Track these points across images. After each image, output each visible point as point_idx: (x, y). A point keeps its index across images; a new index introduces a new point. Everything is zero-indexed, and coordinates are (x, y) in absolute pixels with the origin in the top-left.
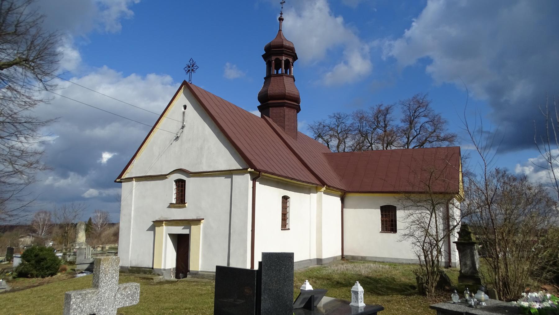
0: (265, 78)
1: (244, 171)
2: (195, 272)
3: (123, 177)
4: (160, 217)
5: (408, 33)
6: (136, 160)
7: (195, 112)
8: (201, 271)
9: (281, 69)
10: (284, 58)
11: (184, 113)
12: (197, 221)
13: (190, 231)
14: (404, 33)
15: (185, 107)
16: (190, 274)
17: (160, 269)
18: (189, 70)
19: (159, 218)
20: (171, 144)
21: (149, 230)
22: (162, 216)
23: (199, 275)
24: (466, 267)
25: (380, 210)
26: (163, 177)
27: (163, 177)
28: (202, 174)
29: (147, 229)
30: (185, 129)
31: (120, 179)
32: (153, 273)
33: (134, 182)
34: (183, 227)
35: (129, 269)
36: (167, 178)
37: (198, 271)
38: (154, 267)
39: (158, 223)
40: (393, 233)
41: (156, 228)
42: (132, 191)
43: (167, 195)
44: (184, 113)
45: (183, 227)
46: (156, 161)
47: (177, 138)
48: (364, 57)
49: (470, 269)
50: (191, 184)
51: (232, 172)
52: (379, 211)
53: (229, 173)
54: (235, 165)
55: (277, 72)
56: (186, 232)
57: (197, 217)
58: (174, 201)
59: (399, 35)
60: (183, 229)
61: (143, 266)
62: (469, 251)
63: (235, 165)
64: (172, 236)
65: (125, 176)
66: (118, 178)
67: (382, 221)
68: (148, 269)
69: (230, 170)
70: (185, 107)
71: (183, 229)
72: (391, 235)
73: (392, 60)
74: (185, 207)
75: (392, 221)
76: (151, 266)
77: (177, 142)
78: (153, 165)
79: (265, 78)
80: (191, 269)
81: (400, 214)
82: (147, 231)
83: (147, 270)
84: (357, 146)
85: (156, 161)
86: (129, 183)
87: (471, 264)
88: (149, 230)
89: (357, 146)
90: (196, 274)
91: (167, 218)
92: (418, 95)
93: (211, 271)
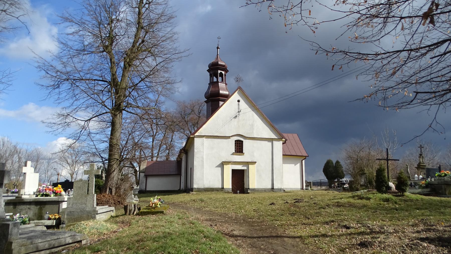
0: (209, 84)
3: (195, 135)
7: (246, 105)
10: (219, 71)
11: (239, 104)
13: (248, 168)
15: (239, 101)
16: (250, 190)
17: (229, 188)
18: (237, 81)
22: (227, 159)
26: (229, 137)
27: (229, 137)
29: (216, 166)
30: (240, 113)
33: (204, 139)
35: (204, 189)
36: (230, 138)
39: (228, 163)
44: (239, 104)
46: (221, 128)
47: (236, 116)
50: (247, 144)
53: (271, 140)
54: (274, 136)
56: (245, 168)
58: (234, 152)
62: (363, 176)
63: (274, 136)
64: (234, 171)
69: (272, 139)
70: (239, 101)
74: (244, 155)
79: (209, 84)
84: (102, 160)
85: (221, 128)
89: (102, 160)
90: (254, 190)
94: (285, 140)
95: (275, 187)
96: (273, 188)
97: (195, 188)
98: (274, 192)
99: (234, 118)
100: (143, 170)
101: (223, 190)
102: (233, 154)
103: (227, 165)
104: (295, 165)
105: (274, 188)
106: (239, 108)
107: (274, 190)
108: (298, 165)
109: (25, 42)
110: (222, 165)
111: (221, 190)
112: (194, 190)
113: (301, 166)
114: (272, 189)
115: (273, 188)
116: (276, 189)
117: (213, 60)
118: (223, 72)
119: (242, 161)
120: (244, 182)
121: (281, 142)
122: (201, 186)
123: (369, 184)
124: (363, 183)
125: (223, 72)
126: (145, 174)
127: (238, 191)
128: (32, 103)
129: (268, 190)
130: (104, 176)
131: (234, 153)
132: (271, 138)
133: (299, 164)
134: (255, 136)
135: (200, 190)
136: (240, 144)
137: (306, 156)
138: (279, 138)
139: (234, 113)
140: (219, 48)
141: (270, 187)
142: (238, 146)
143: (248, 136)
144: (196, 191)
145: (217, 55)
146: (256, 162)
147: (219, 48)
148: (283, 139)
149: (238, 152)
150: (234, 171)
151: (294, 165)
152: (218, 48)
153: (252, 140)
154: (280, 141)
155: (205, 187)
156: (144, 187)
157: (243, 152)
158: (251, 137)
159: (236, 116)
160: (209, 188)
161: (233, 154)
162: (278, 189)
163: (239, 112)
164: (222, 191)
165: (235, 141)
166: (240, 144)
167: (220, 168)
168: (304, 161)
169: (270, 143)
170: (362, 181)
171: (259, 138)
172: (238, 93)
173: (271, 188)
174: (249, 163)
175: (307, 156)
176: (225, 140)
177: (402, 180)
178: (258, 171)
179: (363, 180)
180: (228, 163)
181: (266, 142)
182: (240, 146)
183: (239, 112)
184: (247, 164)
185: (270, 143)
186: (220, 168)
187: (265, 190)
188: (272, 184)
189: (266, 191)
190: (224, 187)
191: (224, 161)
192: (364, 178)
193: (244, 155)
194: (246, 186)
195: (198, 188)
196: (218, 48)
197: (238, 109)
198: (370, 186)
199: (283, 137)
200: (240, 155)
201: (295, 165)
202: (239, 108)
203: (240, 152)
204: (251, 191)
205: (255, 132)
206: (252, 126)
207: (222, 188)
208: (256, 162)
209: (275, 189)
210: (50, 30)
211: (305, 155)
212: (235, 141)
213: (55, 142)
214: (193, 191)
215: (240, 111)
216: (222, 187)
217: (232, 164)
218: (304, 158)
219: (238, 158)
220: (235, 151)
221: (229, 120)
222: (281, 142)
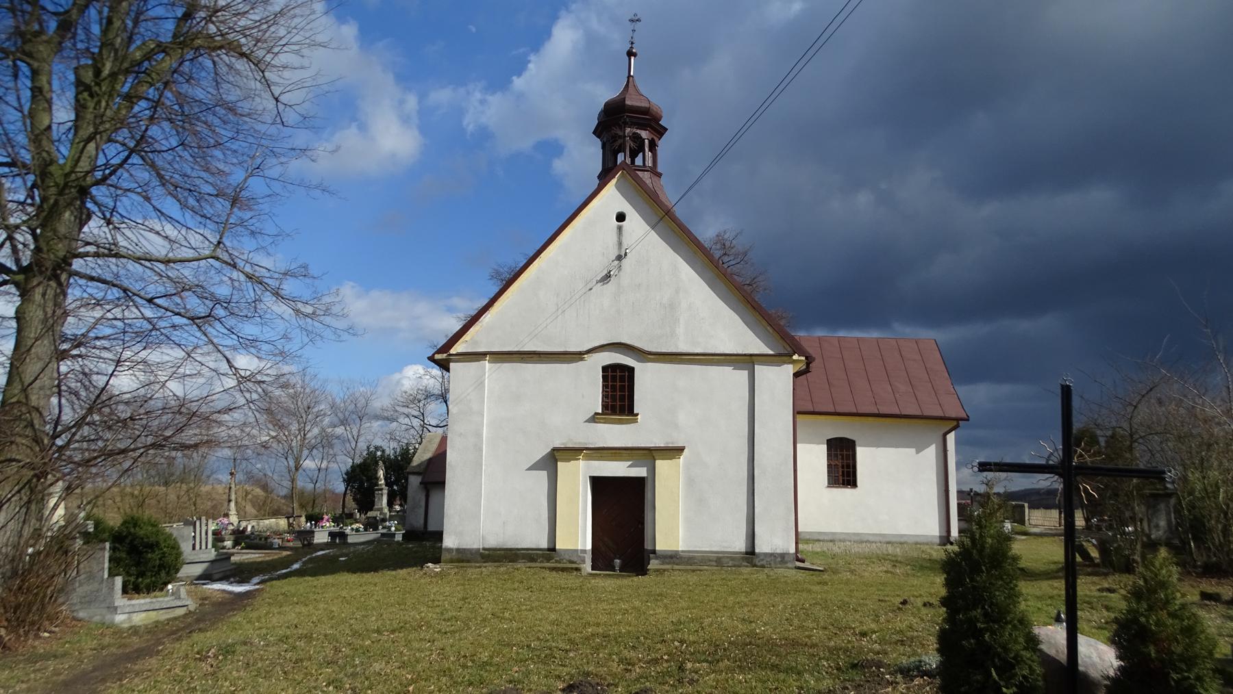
1: (777, 358)
2: (670, 553)
3: (453, 351)
4: (565, 441)
5: (518, 83)
6: (489, 315)
8: (683, 551)
9: (641, 155)
11: (620, 228)
12: (674, 452)
13: (652, 471)
14: (511, 82)
15: (621, 217)
16: (657, 558)
17: (576, 551)
19: (563, 444)
20: (591, 289)
21: (535, 467)
23: (681, 558)
24: (1159, 531)
25: (825, 447)
26: (578, 356)
27: (578, 356)
28: (679, 357)
30: (625, 262)
31: (445, 355)
32: (558, 559)
33: (487, 364)
34: (631, 463)
35: (481, 554)
36: (582, 359)
37: (678, 551)
38: (559, 546)
39: (572, 453)
40: (851, 488)
41: (559, 464)
42: (482, 383)
43: (583, 396)
44: (620, 228)
45: (631, 463)
46: (549, 321)
47: (607, 277)
48: (405, 120)
49: (1165, 532)
50: (647, 378)
51: (754, 358)
52: (824, 448)
53: (747, 361)
54: (756, 345)
55: (633, 162)
56: (641, 472)
57: (667, 443)
58: (600, 412)
59: (499, 82)
60: (629, 466)
61: (520, 547)
63: (756, 345)
64: (598, 484)
65: (458, 348)
66: (439, 352)
67: (829, 466)
68: (503, 552)
69: (751, 355)
70: (621, 217)
71: (629, 466)
72: (847, 492)
73: (484, 135)
74: (635, 421)
75: (848, 466)
76: (544, 544)
77: (605, 286)
78: (540, 329)
80: (660, 546)
81: (864, 455)
82: (529, 469)
83: (537, 554)
85: (549, 321)
86: (473, 366)
87: (1166, 526)
88: (535, 467)
90: (673, 558)
91: (589, 443)
92: (725, 232)
93: (707, 550)
94: (803, 358)
95: (762, 547)
96: (751, 553)
97: (449, 550)
98: (755, 566)
99: (601, 281)
100: (419, 465)
101: (552, 558)
102: (594, 419)
103: (568, 460)
104: (918, 452)
105: (757, 551)
106: (620, 244)
107: (756, 561)
108: (931, 452)
109: (349, 137)
110: (553, 459)
111: (543, 556)
112: (445, 556)
113: (942, 454)
114: (747, 553)
115: (751, 553)
116: (766, 554)
117: (605, 93)
118: (644, 134)
119: (630, 445)
120: (643, 524)
121: (789, 370)
122: (472, 542)
123: (1195, 539)
124: (1161, 533)
125: (644, 134)
126: (422, 479)
127: (617, 562)
128: (351, 283)
129: (732, 559)
130: (382, 476)
131: (597, 414)
132: (745, 355)
133: (933, 448)
134: (683, 348)
135: (464, 557)
136: (622, 379)
137: (958, 420)
138: (782, 351)
139: (601, 259)
140: (635, 55)
141: (740, 545)
142: (614, 388)
143: (654, 350)
144: (452, 561)
145: (629, 76)
146: (681, 450)
147: (635, 55)
148: (795, 357)
149: (614, 413)
150: (598, 484)
151: (913, 450)
152: (630, 54)
153: (671, 362)
154: (784, 363)
155: (487, 546)
156: (422, 521)
157: (635, 412)
158: (664, 350)
159: (607, 277)
160: (500, 549)
161: (594, 419)
162: (771, 555)
163: (619, 258)
164: (549, 559)
165: (605, 369)
166: (622, 379)
167: (545, 473)
168: (951, 438)
169: (744, 374)
170: (1157, 526)
171: (697, 354)
172: (617, 187)
173: (743, 550)
174: (655, 454)
175: (962, 419)
176: (565, 366)
177: (1152, 651)
178: (691, 482)
179: (1163, 523)
180: (572, 453)
181: (727, 371)
182: (622, 388)
183: (619, 258)
184: (649, 455)
185: (744, 374)
186: (545, 473)
187: (719, 561)
188: (751, 533)
189: (725, 560)
190: (557, 547)
191: (558, 444)
192: (1168, 514)
193: (635, 421)
194: (648, 546)
195: (458, 550)
196: (630, 54)
197: (616, 247)
198: (1197, 547)
199: (796, 347)
200: (620, 422)
201: (918, 452)
202: (620, 244)
203: (622, 412)
204: (663, 564)
205: (680, 330)
206: (672, 307)
207: (549, 550)
208: (681, 450)
209: (760, 554)
210: (402, 102)
211: (954, 415)
212: (605, 369)
213: (397, 376)
214: (443, 558)
215: (626, 254)
216: (551, 547)
217: (588, 458)
218: (951, 426)
219: (615, 434)
220: (605, 407)
221: (584, 291)
222: (789, 370)
